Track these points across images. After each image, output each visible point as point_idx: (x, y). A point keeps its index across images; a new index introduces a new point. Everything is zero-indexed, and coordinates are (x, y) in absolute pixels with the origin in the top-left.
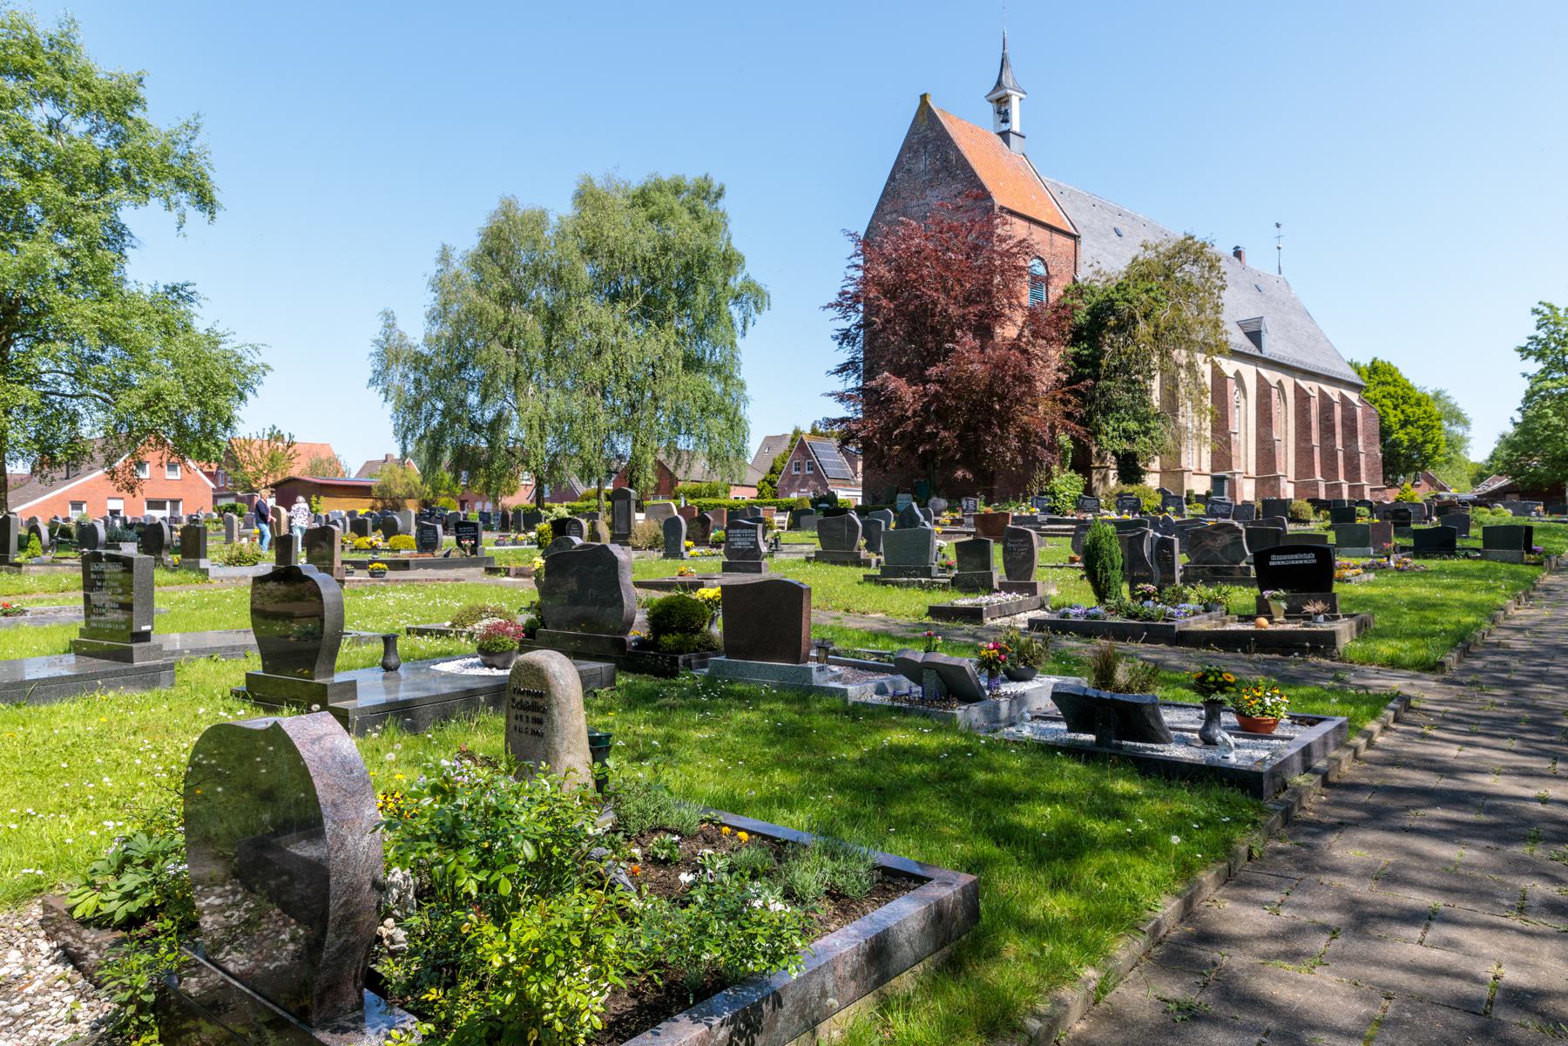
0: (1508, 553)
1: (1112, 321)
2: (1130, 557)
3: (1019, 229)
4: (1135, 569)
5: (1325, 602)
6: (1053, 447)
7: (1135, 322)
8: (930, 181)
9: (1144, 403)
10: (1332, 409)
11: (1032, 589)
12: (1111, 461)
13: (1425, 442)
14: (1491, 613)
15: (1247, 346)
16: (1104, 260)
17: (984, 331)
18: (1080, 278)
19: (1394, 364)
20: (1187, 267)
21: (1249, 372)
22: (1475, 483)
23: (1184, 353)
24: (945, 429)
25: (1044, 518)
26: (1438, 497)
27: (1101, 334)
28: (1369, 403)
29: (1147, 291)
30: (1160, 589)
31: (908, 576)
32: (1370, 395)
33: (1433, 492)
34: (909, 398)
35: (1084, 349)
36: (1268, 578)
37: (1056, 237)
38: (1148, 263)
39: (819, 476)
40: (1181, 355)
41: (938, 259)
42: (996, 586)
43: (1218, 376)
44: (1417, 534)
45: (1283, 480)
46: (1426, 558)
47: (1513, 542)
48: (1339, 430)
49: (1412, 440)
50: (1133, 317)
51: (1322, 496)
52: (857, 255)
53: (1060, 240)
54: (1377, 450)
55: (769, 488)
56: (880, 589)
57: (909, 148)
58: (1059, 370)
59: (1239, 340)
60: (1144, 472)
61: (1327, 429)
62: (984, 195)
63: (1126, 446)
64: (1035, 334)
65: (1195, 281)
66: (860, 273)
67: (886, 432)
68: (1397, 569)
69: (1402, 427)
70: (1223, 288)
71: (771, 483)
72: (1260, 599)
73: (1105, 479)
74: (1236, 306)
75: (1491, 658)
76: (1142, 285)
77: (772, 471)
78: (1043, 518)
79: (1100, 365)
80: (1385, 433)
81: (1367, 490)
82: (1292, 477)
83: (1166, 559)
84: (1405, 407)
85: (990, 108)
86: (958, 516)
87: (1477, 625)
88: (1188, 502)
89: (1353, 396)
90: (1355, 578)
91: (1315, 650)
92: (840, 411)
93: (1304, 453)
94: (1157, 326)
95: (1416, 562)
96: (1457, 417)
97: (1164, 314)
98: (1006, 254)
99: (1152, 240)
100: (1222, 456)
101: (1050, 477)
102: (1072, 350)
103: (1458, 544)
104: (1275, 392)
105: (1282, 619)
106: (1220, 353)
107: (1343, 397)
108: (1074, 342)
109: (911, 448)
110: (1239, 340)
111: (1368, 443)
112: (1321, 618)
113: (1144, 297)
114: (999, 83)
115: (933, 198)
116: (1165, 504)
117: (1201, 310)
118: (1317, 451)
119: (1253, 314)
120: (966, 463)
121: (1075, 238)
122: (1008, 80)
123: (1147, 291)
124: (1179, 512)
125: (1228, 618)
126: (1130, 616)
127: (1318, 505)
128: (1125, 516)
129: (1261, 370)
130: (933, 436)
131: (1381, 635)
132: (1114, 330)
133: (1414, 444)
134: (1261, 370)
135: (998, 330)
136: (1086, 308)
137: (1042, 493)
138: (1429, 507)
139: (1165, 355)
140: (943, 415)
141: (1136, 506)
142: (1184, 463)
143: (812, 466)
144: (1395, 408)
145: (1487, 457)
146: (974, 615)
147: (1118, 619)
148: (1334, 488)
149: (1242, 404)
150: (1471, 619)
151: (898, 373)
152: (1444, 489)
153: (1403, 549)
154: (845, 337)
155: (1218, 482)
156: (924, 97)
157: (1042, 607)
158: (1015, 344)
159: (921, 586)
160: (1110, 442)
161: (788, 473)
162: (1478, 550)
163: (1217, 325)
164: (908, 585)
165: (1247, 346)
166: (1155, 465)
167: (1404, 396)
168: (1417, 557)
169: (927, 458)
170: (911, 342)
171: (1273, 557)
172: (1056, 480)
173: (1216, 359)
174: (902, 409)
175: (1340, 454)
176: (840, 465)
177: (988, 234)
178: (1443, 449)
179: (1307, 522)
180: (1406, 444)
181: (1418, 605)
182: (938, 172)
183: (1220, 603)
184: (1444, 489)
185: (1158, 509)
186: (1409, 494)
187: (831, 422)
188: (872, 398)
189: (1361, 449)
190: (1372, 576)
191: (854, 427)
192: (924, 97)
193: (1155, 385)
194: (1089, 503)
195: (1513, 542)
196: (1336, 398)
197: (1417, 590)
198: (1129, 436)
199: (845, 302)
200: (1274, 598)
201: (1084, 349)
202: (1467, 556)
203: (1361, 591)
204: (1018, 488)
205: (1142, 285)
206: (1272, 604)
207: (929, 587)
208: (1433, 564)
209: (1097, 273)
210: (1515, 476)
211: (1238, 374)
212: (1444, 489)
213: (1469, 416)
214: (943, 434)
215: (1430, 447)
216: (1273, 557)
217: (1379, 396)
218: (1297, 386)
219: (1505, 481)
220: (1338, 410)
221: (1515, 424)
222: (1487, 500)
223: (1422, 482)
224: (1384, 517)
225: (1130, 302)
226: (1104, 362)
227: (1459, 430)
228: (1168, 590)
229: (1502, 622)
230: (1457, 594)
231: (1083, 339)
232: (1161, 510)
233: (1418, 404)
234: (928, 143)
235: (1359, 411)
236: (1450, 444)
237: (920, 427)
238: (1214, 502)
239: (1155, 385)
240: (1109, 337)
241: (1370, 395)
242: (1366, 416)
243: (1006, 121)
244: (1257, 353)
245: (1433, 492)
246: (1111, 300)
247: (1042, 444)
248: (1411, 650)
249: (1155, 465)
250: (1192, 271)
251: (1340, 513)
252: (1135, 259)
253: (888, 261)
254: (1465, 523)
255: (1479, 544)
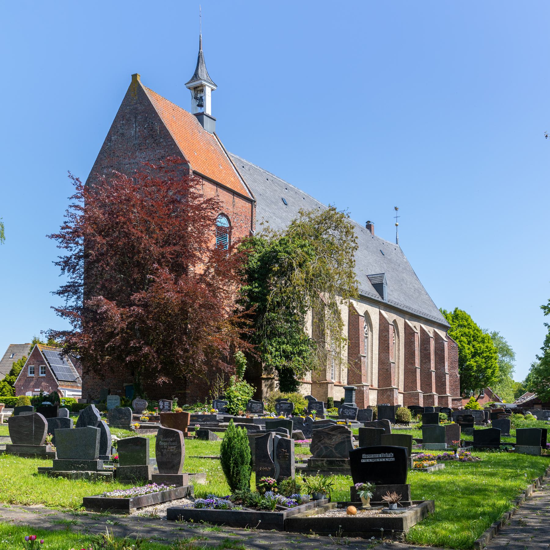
0: (532, 448)
1: (276, 268)
2: (256, 457)
3: (208, 191)
4: (261, 463)
5: (398, 494)
6: (232, 361)
7: (293, 269)
8: (139, 145)
9: (299, 331)
10: (429, 343)
11: (179, 481)
12: (275, 374)
13: (487, 368)
14: (516, 495)
15: (373, 294)
16: (272, 222)
17: (179, 269)
18: (254, 233)
19: (468, 312)
20: (330, 231)
21: (374, 313)
22: (516, 397)
23: (327, 295)
24: (147, 344)
25: (222, 417)
26: (493, 406)
27: (266, 274)
28: (452, 339)
29: (302, 246)
30: (279, 481)
31: (77, 469)
32: (453, 333)
33: (491, 402)
34: (117, 318)
35: (256, 288)
36: (360, 473)
37: (237, 200)
38: (303, 226)
39: (50, 377)
40: (325, 296)
41: (143, 207)
42: (150, 478)
43: (353, 315)
44: (476, 433)
45: (396, 391)
46: (481, 450)
47: (534, 439)
48: (432, 357)
49: (479, 366)
50: (291, 265)
51: (421, 405)
52: (77, 197)
53: (240, 202)
54: (457, 371)
55: (8, 387)
56: (50, 481)
57: (121, 116)
58: (237, 302)
59: (366, 288)
60: (298, 383)
61: (425, 357)
62: (181, 162)
63: (284, 362)
64: (218, 272)
65: (336, 242)
66: (81, 213)
67: (100, 345)
68: (461, 460)
69: (473, 356)
70: (355, 248)
71: (11, 383)
72: (353, 489)
73: (271, 387)
74: (364, 264)
75: (512, 535)
76: (298, 242)
77: (12, 373)
78: (220, 417)
79: (266, 300)
80: (462, 360)
81: (450, 399)
82: (401, 389)
83: (285, 457)
84: (475, 343)
85: (189, 94)
86: (155, 414)
87: (506, 507)
88: (328, 406)
89: (442, 334)
90: (430, 470)
91: (387, 534)
92: (65, 325)
93: (410, 373)
94: (307, 273)
95: (473, 454)
96: (506, 351)
97: (313, 265)
98: (198, 208)
99: (307, 208)
100: (355, 373)
101: (228, 384)
102: (247, 287)
103: (502, 440)
104: (391, 327)
105: (368, 506)
106: (352, 296)
107: (436, 334)
108: (250, 281)
109: (120, 359)
110: (366, 288)
111: (451, 368)
112: (395, 506)
113: (299, 251)
114: (196, 76)
115: (141, 158)
116: (310, 408)
117: (339, 263)
118: (418, 371)
119: (378, 271)
120: (166, 372)
121: (252, 202)
122: (203, 73)
123: (302, 246)
124: (320, 413)
125: (330, 505)
126: (252, 506)
127: (415, 410)
128: (282, 417)
129: (383, 312)
130: (138, 349)
131: (439, 518)
132: (275, 274)
133: (481, 370)
134: (383, 312)
135: (191, 268)
136: (257, 255)
137: (222, 397)
138: (486, 414)
139: (315, 296)
140: (145, 333)
141: (289, 410)
142: (328, 377)
143: (45, 370)
144: (469, 343)
145: (524, 379)
146: (122, 505)
147: (240, 509)
148: (429, 398)
149: (370, 336)
150: (502, 502)
151: (110, 297)
152: (498, 400)
153: (467, 443)
154: (67, 264)
155: (349, 391)
156: (134, 76)
157: (188, 495)
158: (202, 278)
159: (88, 478)
160: (273, 359)
161: (24, 374)
162: (513, 445)
163: (350, 276)
164: (77, 477)
165: (373, 294)
166: (308, 377)
167: (475, 337)
168: (474, 450)
169: (133, 367)
170: (120, 272)
171: (364, 456)
172: (233, 388)
173: (351, 301)
174: (112, 326)
175: (433, 374)
176: (69, 370)
177: (184, 191)
178: (498, 373)
179: (407, 423)
180: (475, 368)
181: (470, 490)
182: (145, 138)
183: (323, 493)
184: (498, 400)
185: (305, 411)
186: (474, 404)
187: (53, 335)
188: (89, 316)
189: (447, 371)
190: (443, 466)
191: (74, 340)
192: (134, 76)
193: (309, 317)
194: (256, 406)
195: (534, 439)
196: (431, 335)
197: (470, 477)
198: (287, 356)
199: (66, 237)
200: (362, 489)
201: (256, 288)
202: (506, 450)
203: (433, 478)
204: (203, 395)
205: (298, 242)
206: (362, 493)
207: (94, 479)
208: (484, 456)
209: (266, 230)
210: (539, 393)
211: (367, 314)
212: (498, 400)
213: (514, 351)
214: (146, 349)
215: (489, 371)
216: (364, 456)
217: (459, 334)
218: (406, 325)
219: (533, 396)
220: (432, 343)
221: (540, 359)
222: (521, 409)
223: (485, 395)
224: (457, 421)
225: (289, 254)
226: (269, 298)
227: (506, 359)
228: (284, 482)
229: (523, 503)
230: (496, 481)
231: (255, 279)
232: (307, 412)
233: (483, 342)
234: (137, 117)
235: (446, 344)
236: (502, 369)
237: (126, 341)
238: (345, 408)
239: (309, 317)
240: (273, 280)
241: (453, 333)
242: (451, 348)
243: (201, 105)
244: (380, 299)
245: (491, 402)
246: (275, 251)
247: (224, 359)
248: (458, 532)
249: (308, 377)
250: (333, 234)
251: (429, 416)
252: (294, 223)
253: (103, 205)
254: (507, 425)
255: (514, 440)
